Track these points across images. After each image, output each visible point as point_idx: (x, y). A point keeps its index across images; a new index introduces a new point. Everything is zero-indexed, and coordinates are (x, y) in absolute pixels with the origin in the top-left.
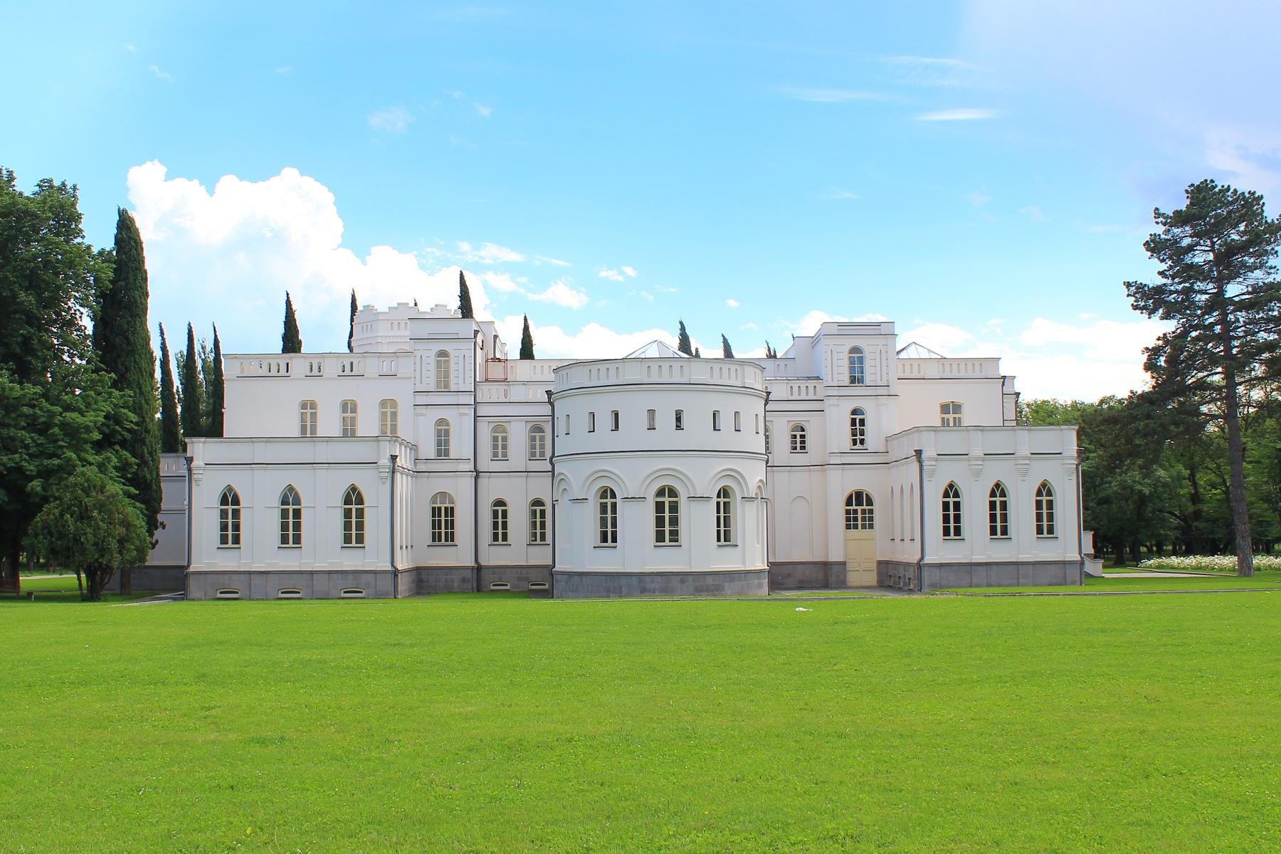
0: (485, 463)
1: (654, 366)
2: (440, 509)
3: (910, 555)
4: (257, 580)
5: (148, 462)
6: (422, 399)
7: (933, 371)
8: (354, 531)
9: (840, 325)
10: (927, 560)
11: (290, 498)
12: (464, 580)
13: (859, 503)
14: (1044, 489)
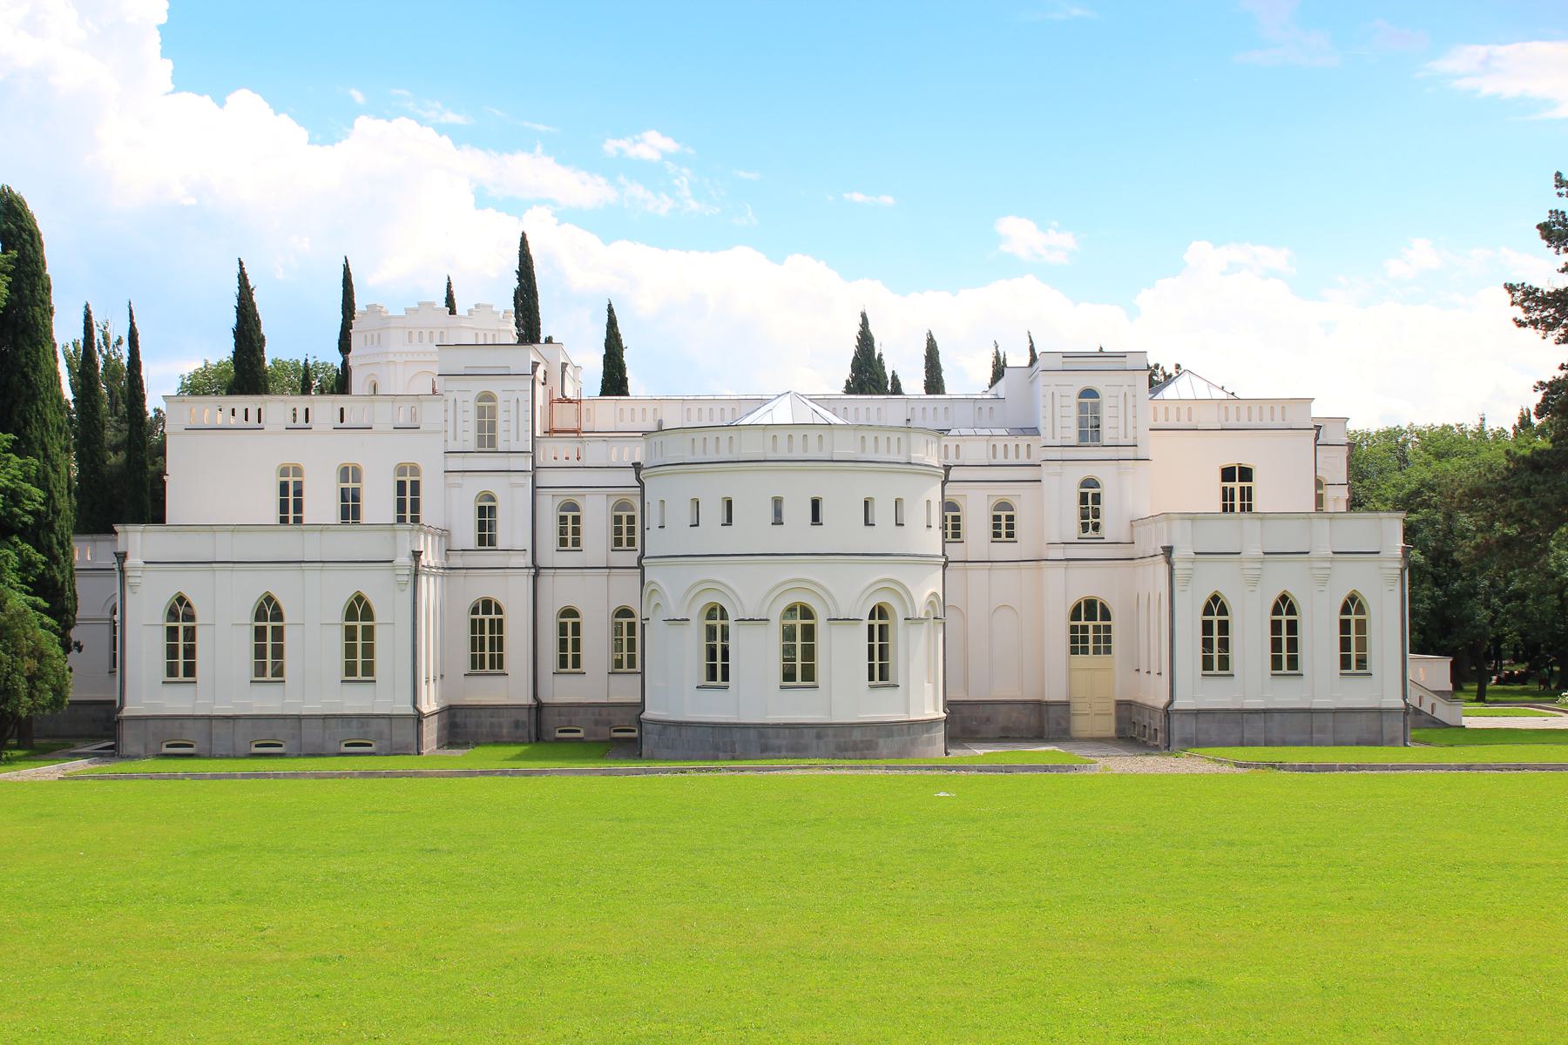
0: (549, 553)
1: (782, 436)
2: (482, 621)
3: (1156, 696)
4: (220, 729)
5: (56, 555)
6: (456, 463)
7: (1211, 418)
8: (359, 659)
9: (1066, 356)
10: (1179, 704)
11: (269, 610)
12: (517, 725)
13: (1091, 616)
14: (1352, 604)
